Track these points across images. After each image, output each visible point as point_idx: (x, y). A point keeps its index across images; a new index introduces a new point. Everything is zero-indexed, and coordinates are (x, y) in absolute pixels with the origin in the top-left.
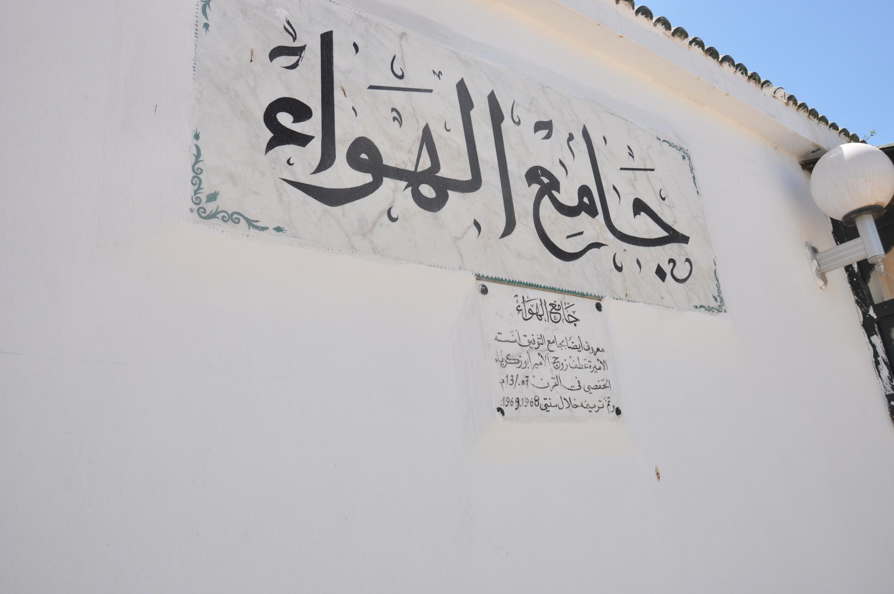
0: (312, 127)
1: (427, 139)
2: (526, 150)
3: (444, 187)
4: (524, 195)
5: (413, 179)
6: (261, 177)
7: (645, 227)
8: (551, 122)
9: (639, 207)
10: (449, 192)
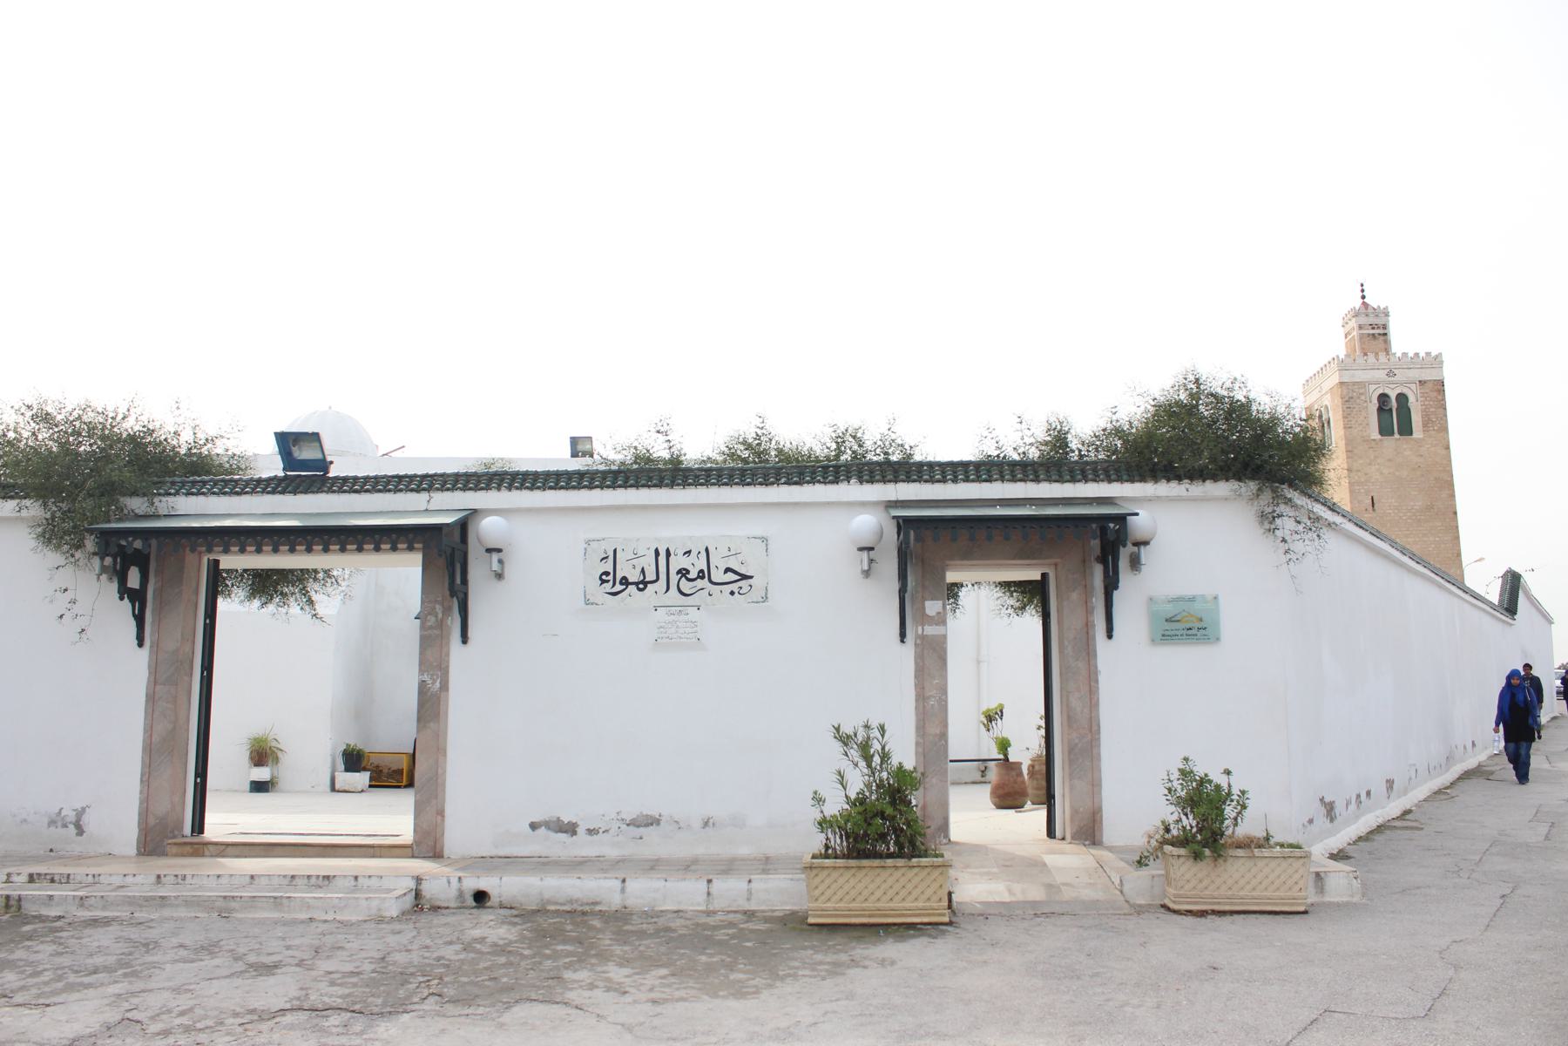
0: (611, 577)
1: (643, 571)
2: (678, 562)
3: (646, 584)
4: (674, 578)
5: (637, 584)
6: (599, 593)
7: (731, 577)
8: (1439, 356)
9: (728, 570)
10: (331, 475)
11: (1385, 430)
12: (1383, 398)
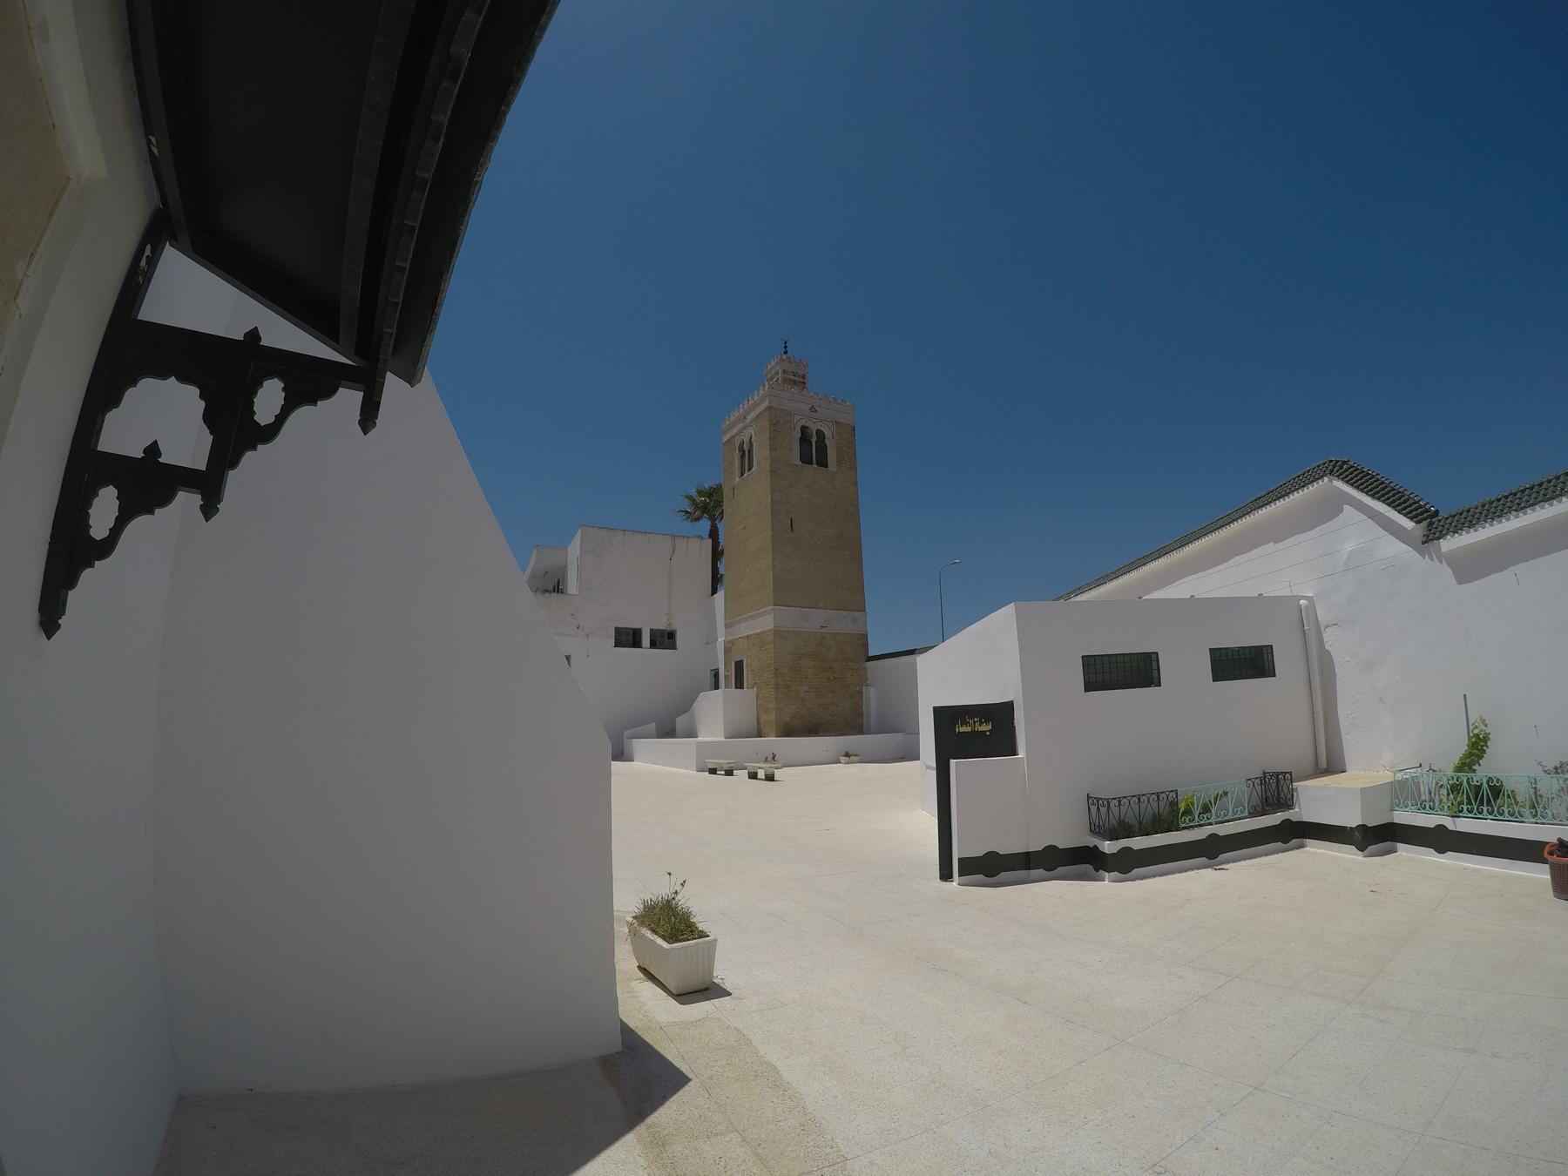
11: (806, 459)
12: (804, 428)
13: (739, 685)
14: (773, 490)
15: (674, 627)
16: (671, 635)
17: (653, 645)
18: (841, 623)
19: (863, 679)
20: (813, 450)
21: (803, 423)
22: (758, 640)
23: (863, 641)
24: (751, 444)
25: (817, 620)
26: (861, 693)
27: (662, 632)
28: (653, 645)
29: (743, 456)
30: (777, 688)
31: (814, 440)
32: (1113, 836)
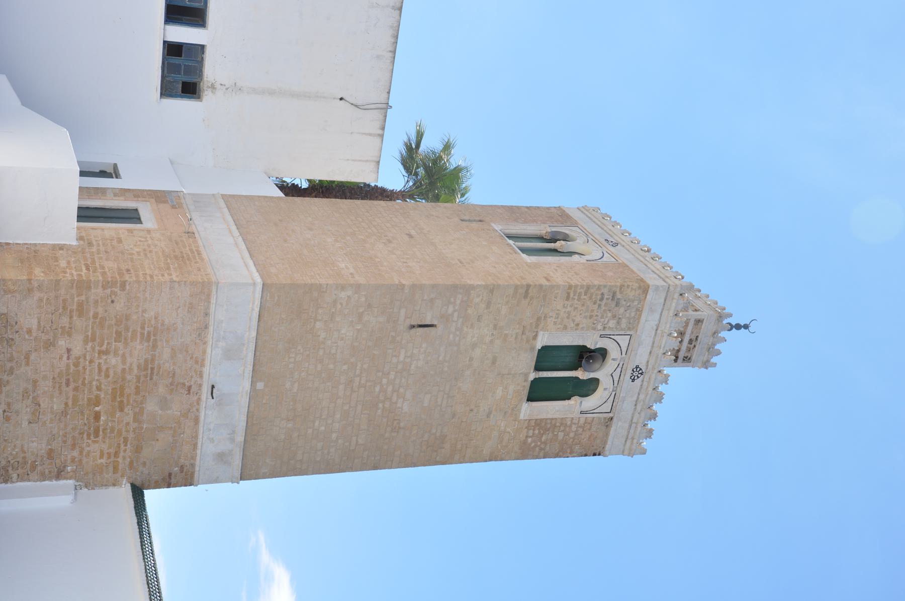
11: (547, 357)
12: (602, 354)
13: (85, 214)
14: (492, 289)
15: (207, 95)
16: (190, 90)
17: (173, 50)
18: (219, 427)
19: (90, 479)
20: (564, 372)
21: (614, 353)
22: (185, 253)
23: (180, 475)
24: (571, 254)
25: (229, 373)
26: (59, 475)
27: (197, 68)
28: (173, 50)
29: (541, 239)
30: (82, 286)
31: (581, 374)
32: (103, 344)
